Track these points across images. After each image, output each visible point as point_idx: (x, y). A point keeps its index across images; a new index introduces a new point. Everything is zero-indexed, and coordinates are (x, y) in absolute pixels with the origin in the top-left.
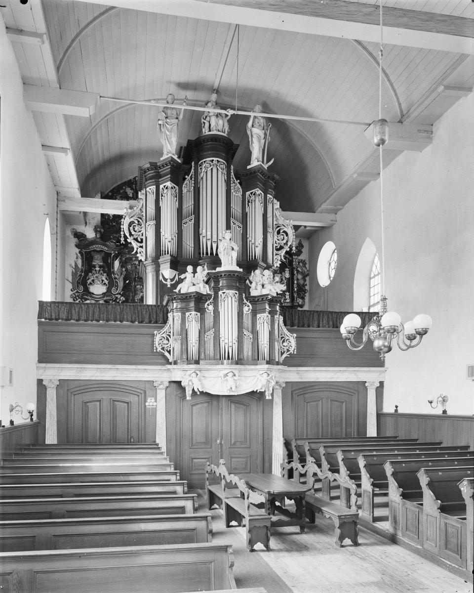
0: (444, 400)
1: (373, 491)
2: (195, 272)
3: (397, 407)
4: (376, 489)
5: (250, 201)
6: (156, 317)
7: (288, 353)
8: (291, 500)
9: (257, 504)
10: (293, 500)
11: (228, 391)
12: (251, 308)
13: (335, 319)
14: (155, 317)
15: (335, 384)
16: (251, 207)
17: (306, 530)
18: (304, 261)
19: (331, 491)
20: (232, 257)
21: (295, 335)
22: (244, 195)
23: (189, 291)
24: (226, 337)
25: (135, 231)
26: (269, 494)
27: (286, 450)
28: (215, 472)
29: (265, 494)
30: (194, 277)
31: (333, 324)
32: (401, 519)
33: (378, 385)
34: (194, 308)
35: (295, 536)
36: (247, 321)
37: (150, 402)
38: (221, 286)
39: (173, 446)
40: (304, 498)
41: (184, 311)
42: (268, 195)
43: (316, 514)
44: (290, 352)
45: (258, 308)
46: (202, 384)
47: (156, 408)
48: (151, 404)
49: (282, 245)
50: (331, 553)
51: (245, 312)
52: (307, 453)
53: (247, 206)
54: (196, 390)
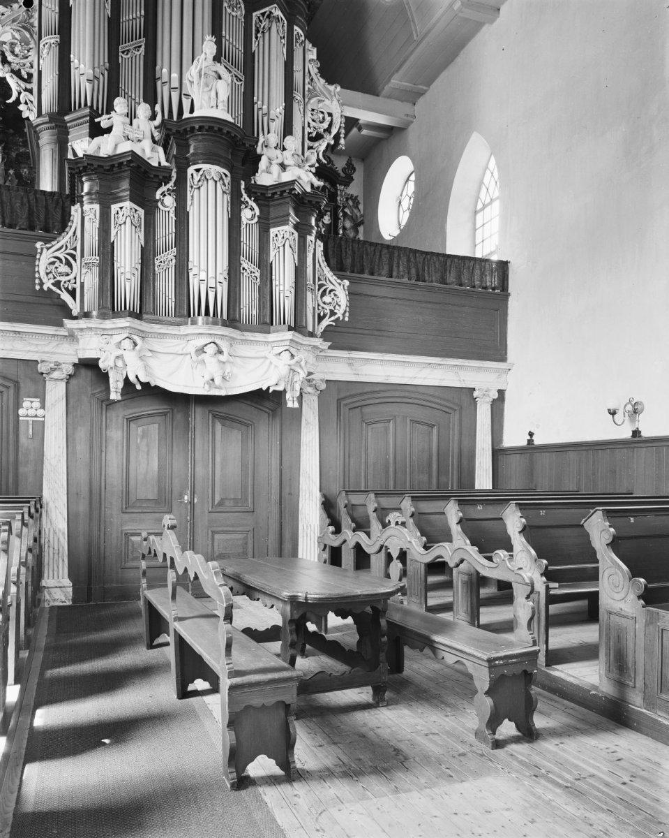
0: (636, 411)
1: (548, 588)
2: (131, 115)
3: (531, 434)
4: (552, 585)
5: (261, 30)
6: (46, 219)
7: (333, 318)
8: (344, 617)
9: (262, 629)
10: (350, 617)
11: (207, 386)
12: (258, 213)
13: (420, 266)
14: (42, 217)
15: (421, 390)
16: (261, 43)
17: (388, 695)
18: (356, 197)
19: (429, 594)
20: (217, 94)
21: (346, 283)
22: (248, 17)
23: (119, 151)
24: (203, 266)
25: (17, 56)
26: (291, 603)
27: (325, 516)
28: (196, 577)
29: (280, 605)
30: (131, 124)
31: (418, 275)
32: (638, 656)
33: (496, 396)
34: (128, 193)
35: (361, 717)
36: (249, 240)
37: (29, 408)
38: (193, 154)
39: (82, 507)
40: (385, 612)
41: (106, 200)
42: (295, 27)
43: (407, 650)
44: (336, 316)
45: (272, 215)
46: (146, 367)
47: (44, 422)
48: (32, 412)
49: (321, 131)
50: (477, 774)
51: (244, 221)
52: (373, 517)
53: (254, 39)
54: (132, 378)
